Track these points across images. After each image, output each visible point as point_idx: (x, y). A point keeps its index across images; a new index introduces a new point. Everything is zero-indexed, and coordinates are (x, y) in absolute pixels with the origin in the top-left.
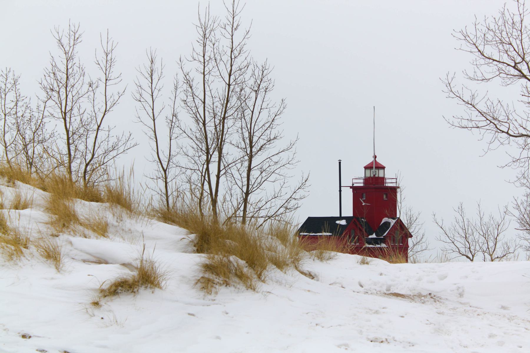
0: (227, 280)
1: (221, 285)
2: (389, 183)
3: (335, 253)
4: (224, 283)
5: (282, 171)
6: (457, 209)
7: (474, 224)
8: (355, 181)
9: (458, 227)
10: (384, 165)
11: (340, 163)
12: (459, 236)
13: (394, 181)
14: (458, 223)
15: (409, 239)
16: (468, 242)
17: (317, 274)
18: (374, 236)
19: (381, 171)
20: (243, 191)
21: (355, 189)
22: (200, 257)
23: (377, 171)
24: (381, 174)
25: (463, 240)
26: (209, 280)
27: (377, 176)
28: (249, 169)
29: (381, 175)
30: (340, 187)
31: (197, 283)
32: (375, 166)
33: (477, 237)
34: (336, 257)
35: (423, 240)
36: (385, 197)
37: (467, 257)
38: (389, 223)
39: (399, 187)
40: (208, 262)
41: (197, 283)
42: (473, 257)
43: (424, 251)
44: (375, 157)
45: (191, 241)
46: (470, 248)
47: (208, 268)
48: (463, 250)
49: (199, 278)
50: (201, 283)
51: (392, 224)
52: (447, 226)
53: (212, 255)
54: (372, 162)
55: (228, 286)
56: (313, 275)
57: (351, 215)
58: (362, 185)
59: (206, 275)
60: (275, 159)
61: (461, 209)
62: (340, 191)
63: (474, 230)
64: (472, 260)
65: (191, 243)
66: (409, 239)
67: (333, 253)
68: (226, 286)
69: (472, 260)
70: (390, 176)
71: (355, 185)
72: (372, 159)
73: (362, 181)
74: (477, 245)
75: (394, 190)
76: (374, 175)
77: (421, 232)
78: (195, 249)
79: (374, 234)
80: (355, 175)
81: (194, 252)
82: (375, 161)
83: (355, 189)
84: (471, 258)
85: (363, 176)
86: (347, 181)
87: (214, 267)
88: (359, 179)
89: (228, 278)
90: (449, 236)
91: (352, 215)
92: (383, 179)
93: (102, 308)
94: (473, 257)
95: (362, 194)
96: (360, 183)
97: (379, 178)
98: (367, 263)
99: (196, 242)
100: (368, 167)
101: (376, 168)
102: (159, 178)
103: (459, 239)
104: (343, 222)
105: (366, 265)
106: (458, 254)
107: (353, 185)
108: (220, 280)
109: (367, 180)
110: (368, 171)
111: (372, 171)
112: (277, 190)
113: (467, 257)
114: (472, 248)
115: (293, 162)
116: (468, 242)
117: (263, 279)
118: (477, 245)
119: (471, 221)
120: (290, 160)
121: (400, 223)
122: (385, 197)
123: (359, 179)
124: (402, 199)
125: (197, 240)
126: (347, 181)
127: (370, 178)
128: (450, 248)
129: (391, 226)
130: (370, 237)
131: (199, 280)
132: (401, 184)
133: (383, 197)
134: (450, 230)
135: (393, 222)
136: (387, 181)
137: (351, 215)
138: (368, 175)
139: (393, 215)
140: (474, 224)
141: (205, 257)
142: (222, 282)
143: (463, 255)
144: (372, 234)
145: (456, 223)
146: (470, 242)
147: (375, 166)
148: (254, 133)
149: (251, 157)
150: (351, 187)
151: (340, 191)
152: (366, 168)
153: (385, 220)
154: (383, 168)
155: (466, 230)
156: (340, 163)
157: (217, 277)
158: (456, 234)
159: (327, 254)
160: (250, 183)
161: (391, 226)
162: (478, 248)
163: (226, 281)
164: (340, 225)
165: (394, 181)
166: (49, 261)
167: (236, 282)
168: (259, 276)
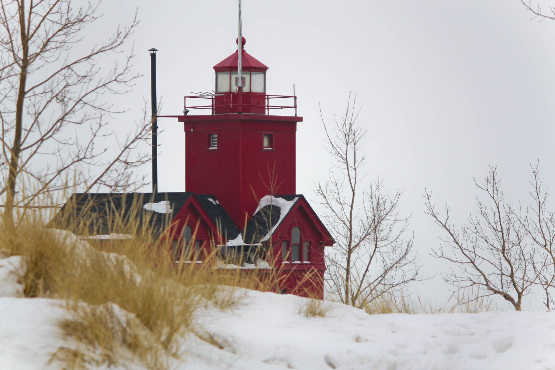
0: (110, 354)
1: (98, 363)
2: (274, 110)
3: (244, 290)
4: (104, 361)
5: (101, 98)
6: (483, 183)
7: (523, 218)
8: (191, 102)
9: (483, 222)
11: (153, 56)
12: (487, 245)
13: (290, 102)
14: (485, 215)
15: (328, 250)
16: (509, 262)
17: (230, 339)
18: (239, 241)
19: (257, 78)
20: (4, 144)
21: (190, 122)
22: (53, 305)
23: (247, 77)
24: (256, 84)
25: (496, 257)
26: (75, 354)
27: (246, 89)
28: (22, 93)
29: (257, 88)
31: (51, 361)
32: (241, 64)
33: (527, 250)
34: (246, 301)
35: (408, 256)
36: (266, 142)
37: (507, 297)
38: (277, 210)
39: (301, 119)
40: (69, 316)
41: (51, 361)
42: (520, 297)
43: (408, 284)
44: (243, 42)
45: (11, 272)
46: (512, 276)
47: (69, 328)
48: (495, 281)
49: (55, 350)
50: (59, 359)
51: (284, 213)
52: (458, 223)
53: (71, 302)
54: (236, 55)
55: (112, 366)
56: (220, 341)
57: (180, 187)
58: (209, 113)
59: (65, 345)
60: (81, 69)
61: (492, 181)
63: (522, 232)
64: (517, 306)
65: (12, 276)
66: (328, 250)
67: (239, 292)
68: (109, 366)
69: (517, 306)
70: (280, 90)
71: (192, 113)
72: (232, 48)
73: (209, 102)
74: (530, 267)
75: (288, 126)
76: (240, 88)
77: (405, 237)
78: (21, 287)
79: (240, 236)
80: (192, 87)
81: (17, 294)
82: (243, 51)
83: (190, 122)
84: (516, 300)
85: (211, 89)
86: (172, 104)
87: (84, 328)
89: (111, 350)
90: (464, 246)
91: (184, 191)
92: (262, 97)
94: (520, 297)
95: (210, 135)
96: (204, 109)
97: (250, 95)
98: (321, 314)
99: (22, 273)
100: (225, 68)
101: (245, 69)
102: (117, 171)
103: (487, 254)
104: (162, 207)
105: (318, 319)
106: (484, 291)
107: (186, 112)
108: (97, 353)
109: (221, 101)
110: (224, 78)
111: (234, 77)
112: (84, 143)
113: (507, 297)
114: (518, 274)
115: (127, 76)
116: (509, 262)
117: (174, 350)
118: (530, 267)
119: (517, 212)
120: (119, 72)
121: (303, 208)
122: (266, 142)
124: (359, 158)
125: (25, 268)
126: (172, 104)
127: (229, 94)
128: (466, 275)
129: (282, 217)
130: (230, 243)
131: (54, 355)
133: (262, 142)
134: (464, 231)
135: (286, 206)
136: (272, 102)
137: (180, 187)
138: (224, 88)
139: (288, 190)
140: (523, 218)
141: (61, 306)
142: (100, 358)
143: (496, 292)
144: (234, 237)
145: (481, 217)
146: (512, 261)
147: (241, 64)
148: (32, 7)
149: (25, 63)
150: (181, 119)
152: (219, 69)
153: (265, 201)
154: (262, 69)
155: (505, 231)
156: (153, 56)
157: (91, 347)
158: (481, 243)
159: (225, 292)
160: (23, 126)
161: (282, 217)
162: (531, 275)
163: (108, 356)
164: (154, 213)
165: (290, 102)
167: (126, 358)
168: (166, 344)
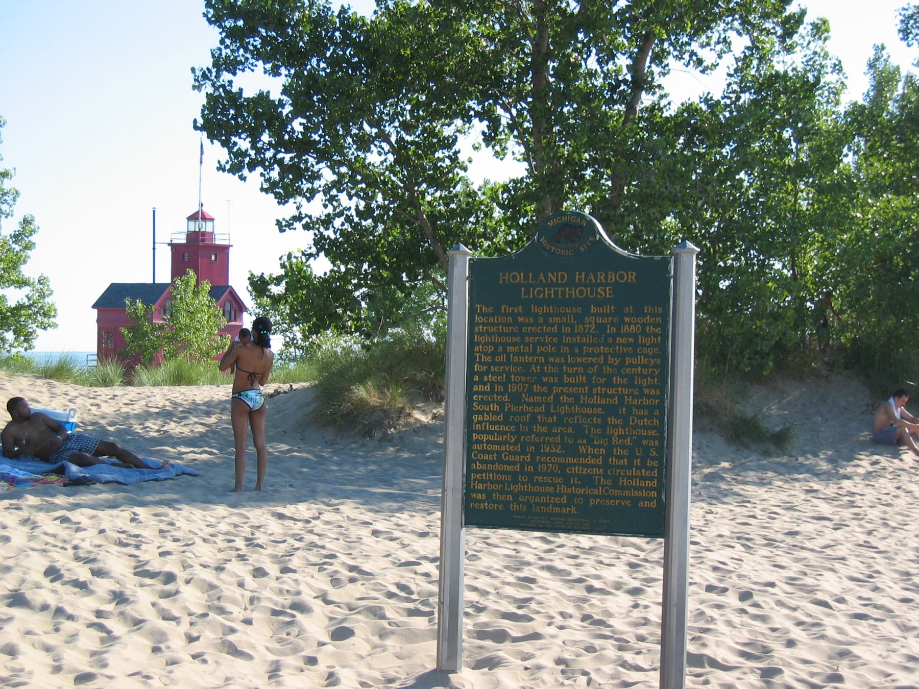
8: (174, 236)
10: (214, 216)
13: (226, 237)
19: (209, 224)
21: (175, 247)
30: (154, 243)
54: (197, 213)
62: (154, 249)
83: (175, 247)
88: (180, 233)
93: (313, 614)
97: (204, 234)
100: (193, 218)
110: (192, 224)
123: (180, 233)
132: (29, 261)
138: (192, 229)
150: (169, 244)
151: (154, 249)
154: (212, 220)
166: (55, 363)
